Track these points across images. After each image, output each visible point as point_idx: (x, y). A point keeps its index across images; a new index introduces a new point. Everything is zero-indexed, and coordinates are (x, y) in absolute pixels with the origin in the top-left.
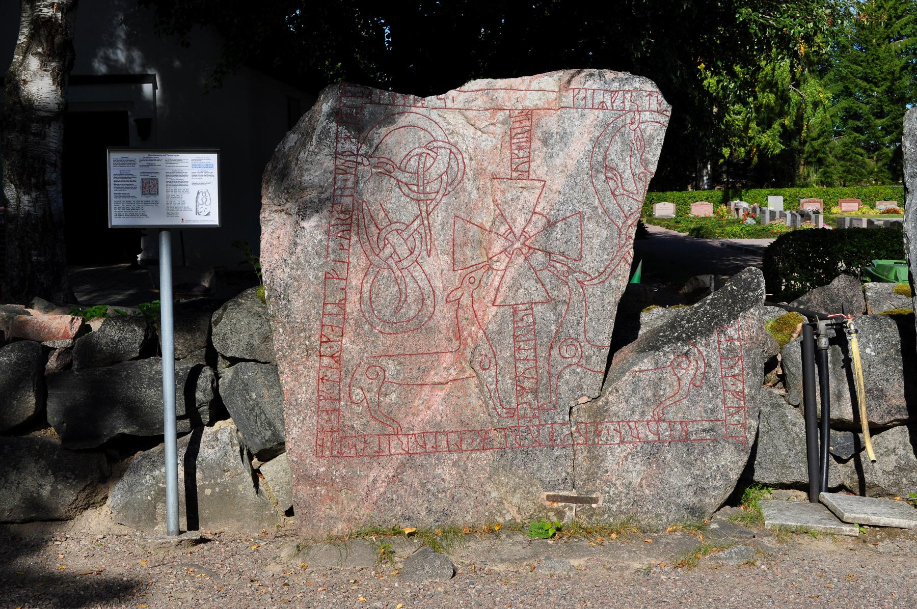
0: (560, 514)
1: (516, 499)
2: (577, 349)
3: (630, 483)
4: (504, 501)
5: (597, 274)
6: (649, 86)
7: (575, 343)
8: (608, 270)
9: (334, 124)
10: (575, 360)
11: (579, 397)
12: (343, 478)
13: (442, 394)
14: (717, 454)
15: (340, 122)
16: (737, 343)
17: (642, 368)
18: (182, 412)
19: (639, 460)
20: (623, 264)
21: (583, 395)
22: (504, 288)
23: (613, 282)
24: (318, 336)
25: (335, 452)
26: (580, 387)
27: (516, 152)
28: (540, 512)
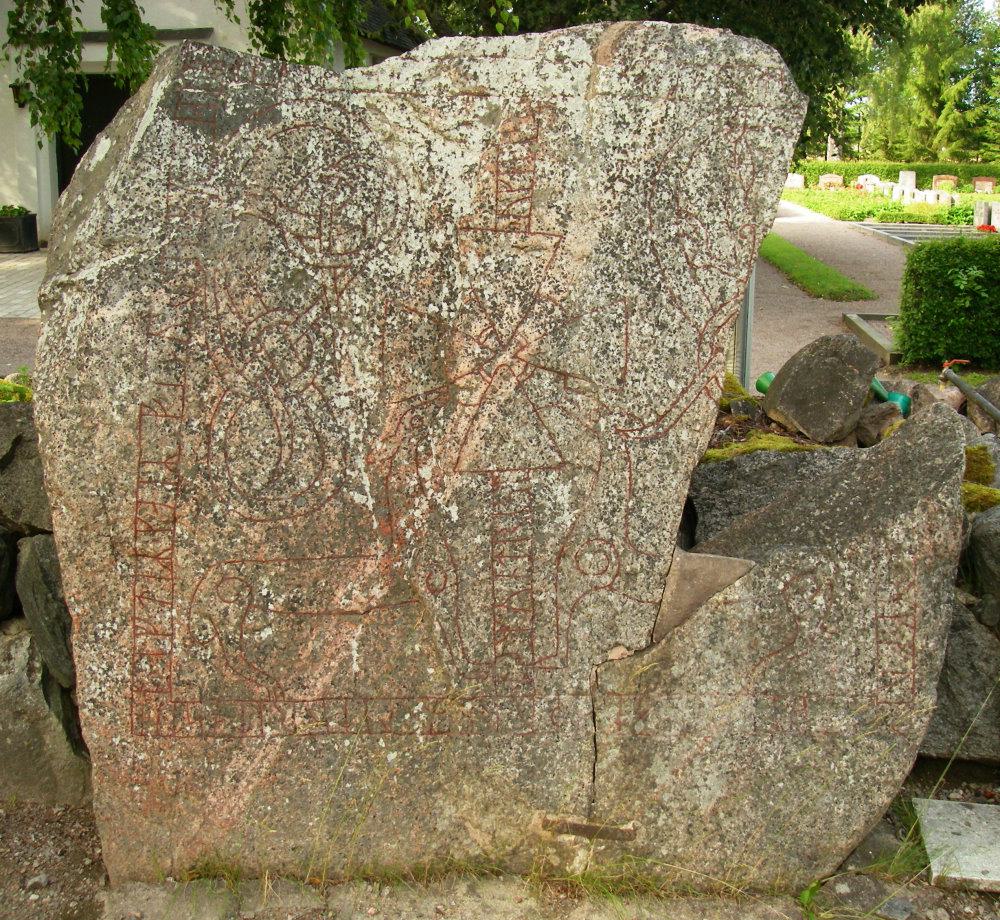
0: (566, 854)
1: (488, 822)
2: (609, 559)
3: (696, 808)
4: (467, 824)
5: (653, 417)
6: (766, 58)
7: (607, 548)
8: (676, 411)
9: (168, 122)
10: (606, 579)
11: (611, 647)
12: (177, 773)
13: (359, 632)
14: (252, 129)
15: (179, 118)
16: (908, 557)
17: (730, 598)
18: (767, 384)
19: (713, 767)
20: (703, 399)
21: (617, 644)
22: (477, 440)
23: (685, 435)
24: (129, 521)
25: (165, 729)
26: (613, 630)
27: (506, 178)
28: (530, 845)
